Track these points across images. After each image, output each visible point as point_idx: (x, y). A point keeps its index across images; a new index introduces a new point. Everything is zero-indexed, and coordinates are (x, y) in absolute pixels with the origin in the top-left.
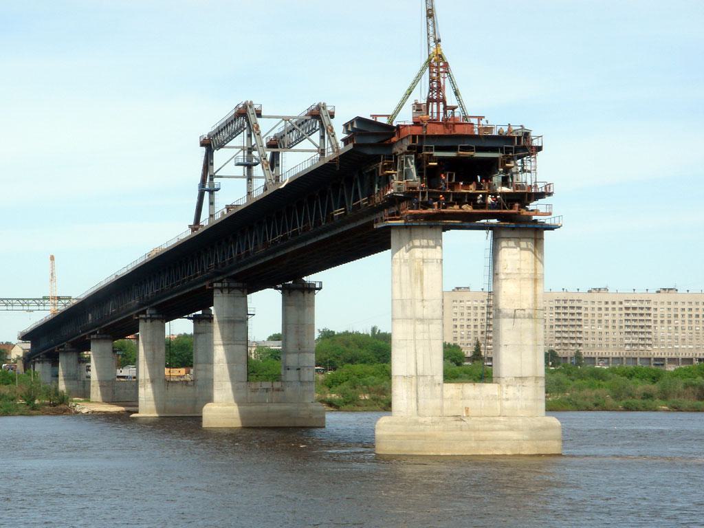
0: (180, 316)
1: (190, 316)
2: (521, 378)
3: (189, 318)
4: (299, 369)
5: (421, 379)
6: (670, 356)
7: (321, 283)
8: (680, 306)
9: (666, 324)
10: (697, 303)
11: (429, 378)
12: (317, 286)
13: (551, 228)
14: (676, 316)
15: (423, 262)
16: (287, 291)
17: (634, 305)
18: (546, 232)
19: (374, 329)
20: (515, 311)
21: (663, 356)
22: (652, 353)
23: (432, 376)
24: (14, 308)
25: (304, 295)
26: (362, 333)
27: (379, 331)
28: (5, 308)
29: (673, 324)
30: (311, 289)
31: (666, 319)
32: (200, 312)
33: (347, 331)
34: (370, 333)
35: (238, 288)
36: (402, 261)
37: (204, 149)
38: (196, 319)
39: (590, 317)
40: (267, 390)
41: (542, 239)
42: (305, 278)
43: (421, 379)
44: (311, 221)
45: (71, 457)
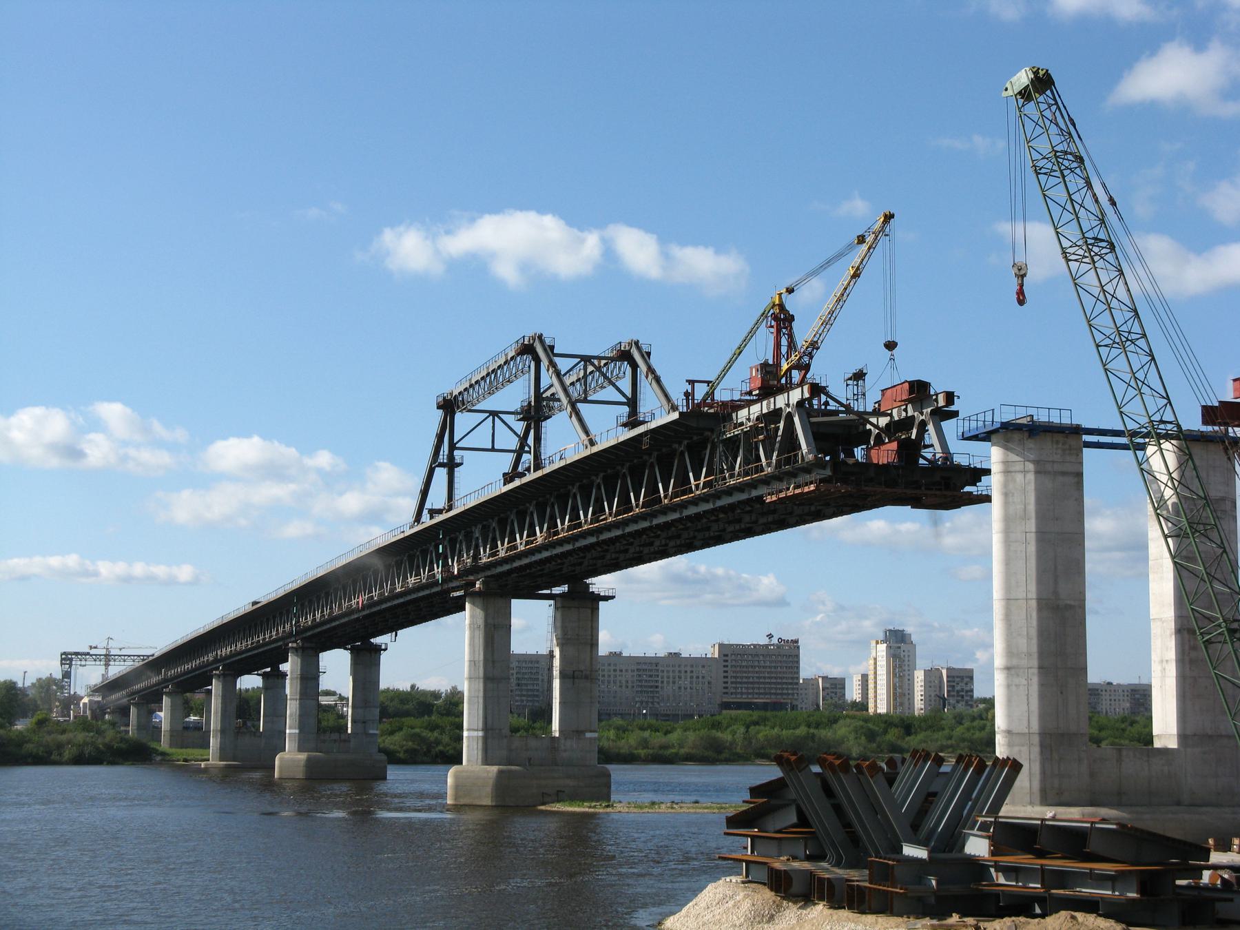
0: (249, 672)
1: (259, 672)
2: (577, 731)
3: (258, 675)
4: (364, 722)
5: (490, 732)
6: (674, 713)
7: (386, 644)
8: (683, 669)
9: (671, 685)
10: (679, 666)
11: (497, 731)
12: (383, 647)
13: (606, 598)
14: (680, 677)
15: (495, 628)
16: (355, 652)
17: (645, 667)
18: (601, 603)
19: (413, 687)
20: (574, 672)
21: (668, 712)
22: (660, 709)
23: (500, 730)
24: (88, 663)
25: (371, 656)
26: (401, 689)
27: (418, 688)
28: (94, 663)
29: (676, 685)
30: (378, 650)
31: (671, 680)
32: (269, 669)
33: (388, 688)
34: (409, 689)
35: (312, 648)
36: (476, 626)
37: (441, 412)
38: (265, 676)
39: (606, 678)
40: (335, 741)
41: (598, 608)
42: (372, 640)
43: (490, 732)
44: (399, 583)
45: (186, 806)
